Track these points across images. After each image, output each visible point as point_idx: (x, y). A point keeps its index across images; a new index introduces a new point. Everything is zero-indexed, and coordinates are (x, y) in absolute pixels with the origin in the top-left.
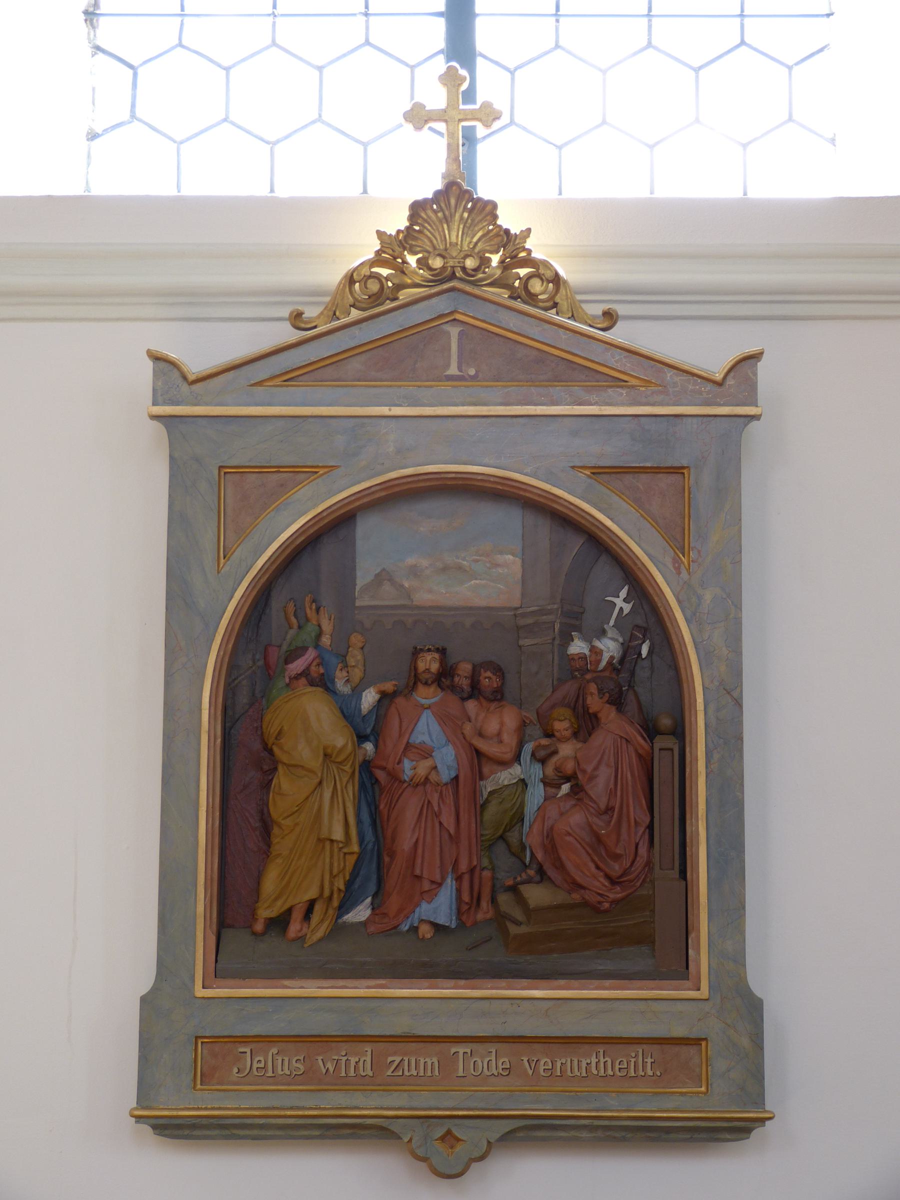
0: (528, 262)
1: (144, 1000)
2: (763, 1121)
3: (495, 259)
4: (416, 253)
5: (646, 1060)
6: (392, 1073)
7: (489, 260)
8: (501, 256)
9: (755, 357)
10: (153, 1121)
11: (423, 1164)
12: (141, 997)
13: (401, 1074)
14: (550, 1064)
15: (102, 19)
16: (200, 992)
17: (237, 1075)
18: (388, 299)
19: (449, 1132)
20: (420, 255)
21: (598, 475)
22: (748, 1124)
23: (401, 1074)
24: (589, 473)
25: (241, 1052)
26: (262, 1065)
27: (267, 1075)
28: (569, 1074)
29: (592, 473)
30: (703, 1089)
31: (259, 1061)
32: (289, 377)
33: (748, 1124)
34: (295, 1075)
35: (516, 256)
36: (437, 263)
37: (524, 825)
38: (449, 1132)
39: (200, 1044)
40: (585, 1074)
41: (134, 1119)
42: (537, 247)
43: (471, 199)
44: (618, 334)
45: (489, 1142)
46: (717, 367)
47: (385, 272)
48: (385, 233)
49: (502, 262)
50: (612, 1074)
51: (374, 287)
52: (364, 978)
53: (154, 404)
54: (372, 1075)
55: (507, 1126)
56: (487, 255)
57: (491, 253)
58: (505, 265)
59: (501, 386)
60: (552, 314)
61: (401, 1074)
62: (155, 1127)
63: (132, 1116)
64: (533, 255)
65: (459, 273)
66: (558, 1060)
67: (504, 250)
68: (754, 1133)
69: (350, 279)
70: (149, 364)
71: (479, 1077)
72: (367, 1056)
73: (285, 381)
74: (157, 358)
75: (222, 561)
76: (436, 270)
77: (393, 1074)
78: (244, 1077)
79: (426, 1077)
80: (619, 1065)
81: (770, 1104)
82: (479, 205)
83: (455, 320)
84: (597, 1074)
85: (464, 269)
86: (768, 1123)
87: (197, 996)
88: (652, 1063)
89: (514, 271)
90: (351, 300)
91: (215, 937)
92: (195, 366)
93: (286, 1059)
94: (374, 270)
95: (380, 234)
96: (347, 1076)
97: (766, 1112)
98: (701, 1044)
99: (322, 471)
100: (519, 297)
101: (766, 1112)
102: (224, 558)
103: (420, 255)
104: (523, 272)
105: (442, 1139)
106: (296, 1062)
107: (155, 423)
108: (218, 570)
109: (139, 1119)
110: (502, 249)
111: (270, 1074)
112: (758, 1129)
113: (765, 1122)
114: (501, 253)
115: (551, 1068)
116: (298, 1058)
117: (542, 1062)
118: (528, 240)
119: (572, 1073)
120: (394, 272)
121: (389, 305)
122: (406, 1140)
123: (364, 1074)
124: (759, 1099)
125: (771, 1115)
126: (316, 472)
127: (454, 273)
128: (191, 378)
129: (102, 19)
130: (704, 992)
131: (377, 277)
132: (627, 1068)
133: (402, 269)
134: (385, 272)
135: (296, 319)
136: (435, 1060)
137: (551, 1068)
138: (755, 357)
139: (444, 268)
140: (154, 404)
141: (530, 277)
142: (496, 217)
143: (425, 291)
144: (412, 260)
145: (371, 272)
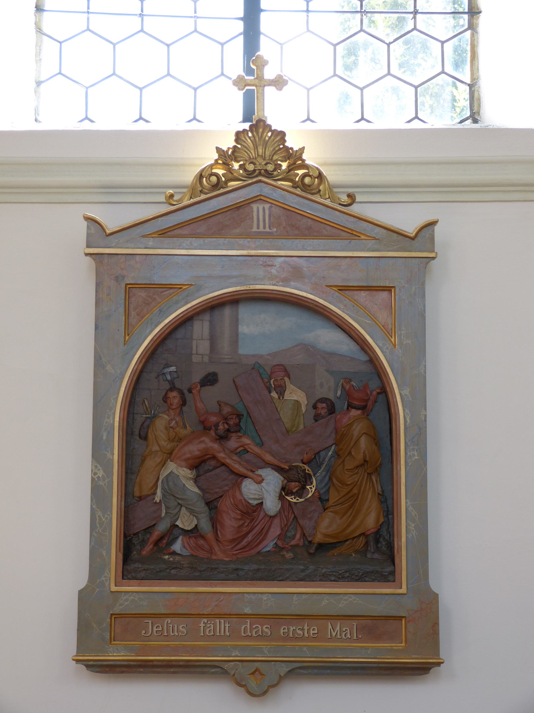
0: (304, 166)
1: (81, 592)
2: (439, 664)
3: (284, 165)
4: (238, 162)
5: (225, 625)
7: (280, 166)
9: (433, 224)
10: (85, 663)
11: (242, 689)
12: (79, 591)
14: (161, 627)
15: (45, 13)
16: (114, 588)
17: (143, 635)
19: (257, 670)
21: (344, 292)
24: (336, 290)
26: (316, 632)
28: (218, 634)
31: (314, 629)
32: (164, 233)
36: (251, 167)
37: (165, 466)
41: (75, 662)
42: (309, 158)
43: (270, 130)
44: (355, 209)
48: (219, 148)
51: (214, 179)
53: (88, 246)
54: (350, 638)
56: (279, 162)
57: (282, 161)
60: (317, 198)
62: (88, 666)
63: (73, 660)
64: (306, 162)
68: (432, 671)
69: (201, 176)
70: (85, 223)
71: (303, 637)
72: (247, 625)
73: (160, 235)
75: (127, 338)
76: (249, 171)
78: (313, 637)
81: (443, 654)
82: (275, 132)
83: (260, 199)
85: (266, 171)
86: (442, 665)
88: (229, 626)
89: (295, 172)
90: (200, 189)
91: (122, 556)
92: (111, 226)
95: (218, 149)
98: (402, 620)
102: (128, 335)
103: (242, 163)
104: (301, 172)
106: (182, 628)
107: (88, 258)
109: (78, 661)
111: (166, 634)
112: (433, 669)
113: (440, 665)
114: (287, 162)
115: (161, 630)
116: (183, 626)
117: (155, 627)
118: (303, 155)
120: (226, 172)
121: (222, 191)
122: (232, 674)
123: (173, 634)
124: (436, 653)
125: (442, 661)
126: (181, 288)
127: (260, 172)
128: (108, 232)
129: (45, 13)
130: (404, 590)
131: (216, 175)
132: (318, 633)
133: (230, 170)
137: (161, 630)
138: (433, 224)
139: (254, 171)
140: (88, 246)
141: (304, 176)
142: (285, 141)
143: (241, 183)
144: (236, 166)
145: (212, 172)
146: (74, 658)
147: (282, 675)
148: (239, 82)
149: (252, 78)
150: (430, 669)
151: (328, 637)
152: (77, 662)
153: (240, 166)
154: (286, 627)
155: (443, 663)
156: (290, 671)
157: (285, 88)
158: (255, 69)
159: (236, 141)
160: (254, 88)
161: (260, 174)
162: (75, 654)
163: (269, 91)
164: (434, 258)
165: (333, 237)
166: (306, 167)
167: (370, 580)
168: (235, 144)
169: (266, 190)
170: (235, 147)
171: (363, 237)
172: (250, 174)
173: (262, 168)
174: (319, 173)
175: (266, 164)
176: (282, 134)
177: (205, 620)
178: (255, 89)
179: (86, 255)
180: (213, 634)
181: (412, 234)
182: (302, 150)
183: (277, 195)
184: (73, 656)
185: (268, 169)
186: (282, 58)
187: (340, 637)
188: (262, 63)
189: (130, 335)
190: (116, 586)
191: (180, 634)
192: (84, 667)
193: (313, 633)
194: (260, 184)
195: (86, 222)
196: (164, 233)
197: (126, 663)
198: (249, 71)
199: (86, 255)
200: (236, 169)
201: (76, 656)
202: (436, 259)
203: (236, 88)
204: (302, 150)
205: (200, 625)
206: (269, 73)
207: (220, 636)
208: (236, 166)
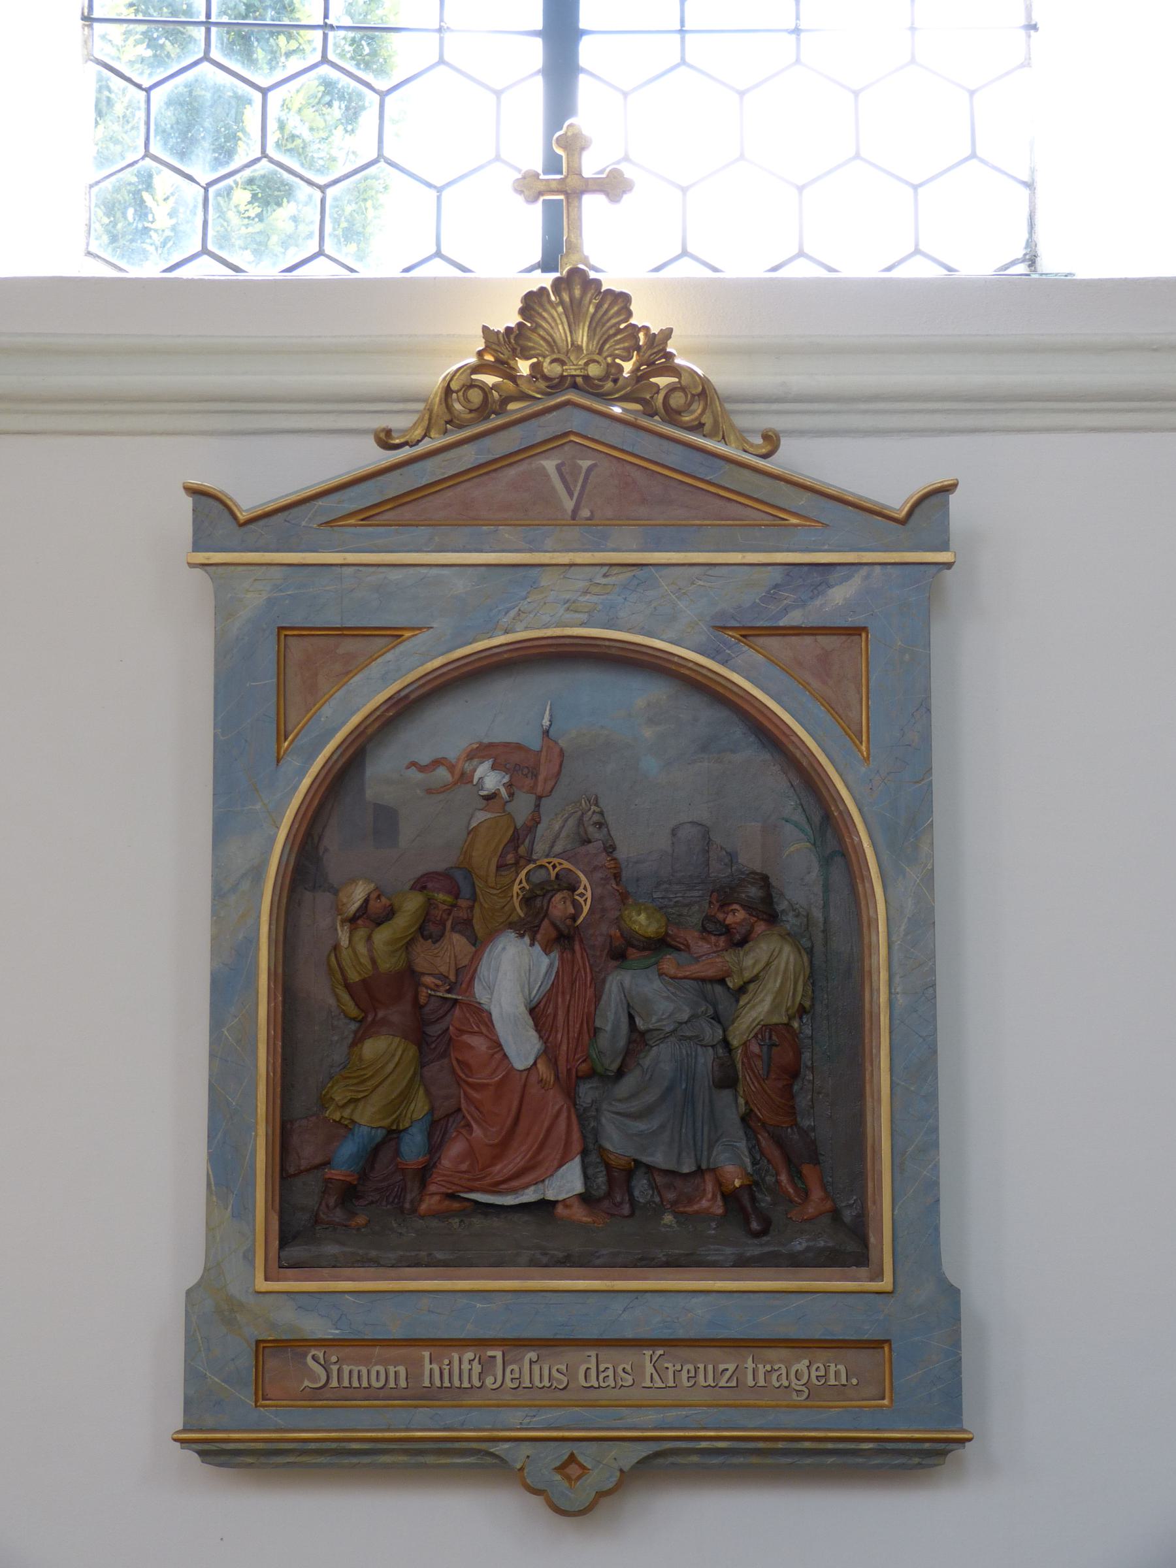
0: (671, 369)
2: (962, 1441)
4: (527, 358)
6: (727, 1382)
8: (634, 363)
9: (947, 489)
10: (195, 1446)
11: (537, 1501)
12: (959, 1290)
13: (734, 1384)
16: (262, 1285)
18: (494, 412)
19: (572, 1458)
20: (535, 360)
22: (942, 1446)
23: (735, 1385)
25: (490, 1357)
26: (822, 1373)
27: (829, 1383)
28: (751, 1383)
29: (741, 636)
30: (886, 1402)
32: (368, 515)
33: (942, 1446)
34: (622, 1386)
35: (653, 363)
38: (572, 1458)
39: (261, 1350)
40: (478, 1382)
41: (178, 1444)
45: (621, 1471)
46: (897, 499)
47: (490, 380)
49: (636, 370)
50: (449, 1385)
51: (476, 396)
52: (417, 1264)
53: (197, 547)
55: (644, 1450)
58: (639, 374)
59: (764, 526)
61: (735, 1385)
62: (202, 1454)
63: (175, 1440)
65: (579, 380)
66: (669, 1365)
67: (638, 354)
70: (188, 502)
71: (504, 1386)
73: (362, 520)
74: (195, 492)
76: (555, 379)
77: (728, 1385)
79: (717, 1388)
80: (816, 1370)
84: (459, 1386)
85: (586, 378)
86: (967, 1444)
87: (892, 1287)
93: (701, 1366)
94: (474, 377)
96: (472, 1387)
97: (965, 1431)
98: (883, 1348)
99: (407, 634)
100: (657, 414)
101: (965, 1431)
103: (535, 360)
104: (662, 381)
105: (561, 1468)
107: (198, 571)
108: (278, 753)
109: (182, 1441)
110: (635, 353)
119: (586, 1382)
120: (501, 380)
123: (540, 1385)
125: (970, 1436)
128: (242, 517)
130: (886, 1284)
131: (482, 387)
133: (512, 376)
134: (490, 380)
135: (385, 440)
136: (402, 1370)
138: (947, 489)
140: (197, 547)
141: (672, 389)
144: (524, 367)
146: (175, 1436)
147: (626, 1469)
148: (529, 187)
149: (558, 177)
150: (943, 1453)
151: (644, 1385)
152: (183, 1445)
153: (533, 366)
154: (610, 1366)
155: (970, 1440)
156: (648, 1458)
157: (626, 198)
158: (561, 157)
159: (523, 312)
160: (561, 197)
161: (575, 386)
162: (181, 1427)
163: (592, 204)
164: (949, 565)
165: (733, 520)
166: (675, 371)
167: (545, 1260)
168: (519, 319)
169: (576, 421)
170: (520, 325)
171: (794, 521)
172: (558, 384)
173: (578, 372)
174: (703, 388)
175: (587, 364)
176: (622, 300)
177: (532, 1355)
178: (544, 200)
179: (192, 565)
180: (613, 1385)
181: (901, 510)
182: (667, 334)
183: (596, 429)
184: (178, 1432)
185: (591, 374)
186: (892, 175)
187: (531, 1386)
188: (575, 144)
189: (290, 738)
190: (266, 1279)
191: (555, 1384)
192: (196, 1455)
193: (817, 1376)
194: (569, 408)
195: (191, 499)
196: (368, 515)
197: (334, 1446)
198: (553, 163)
199: (192, 565)
200: (525, 374)
201: (185, 1430)
202: (954, 567)
203: (520, 199)
204: (667, 334)
205: (746, 1366)
206: (591, 165)
207: (351, 1387)
208: (524, 367)
